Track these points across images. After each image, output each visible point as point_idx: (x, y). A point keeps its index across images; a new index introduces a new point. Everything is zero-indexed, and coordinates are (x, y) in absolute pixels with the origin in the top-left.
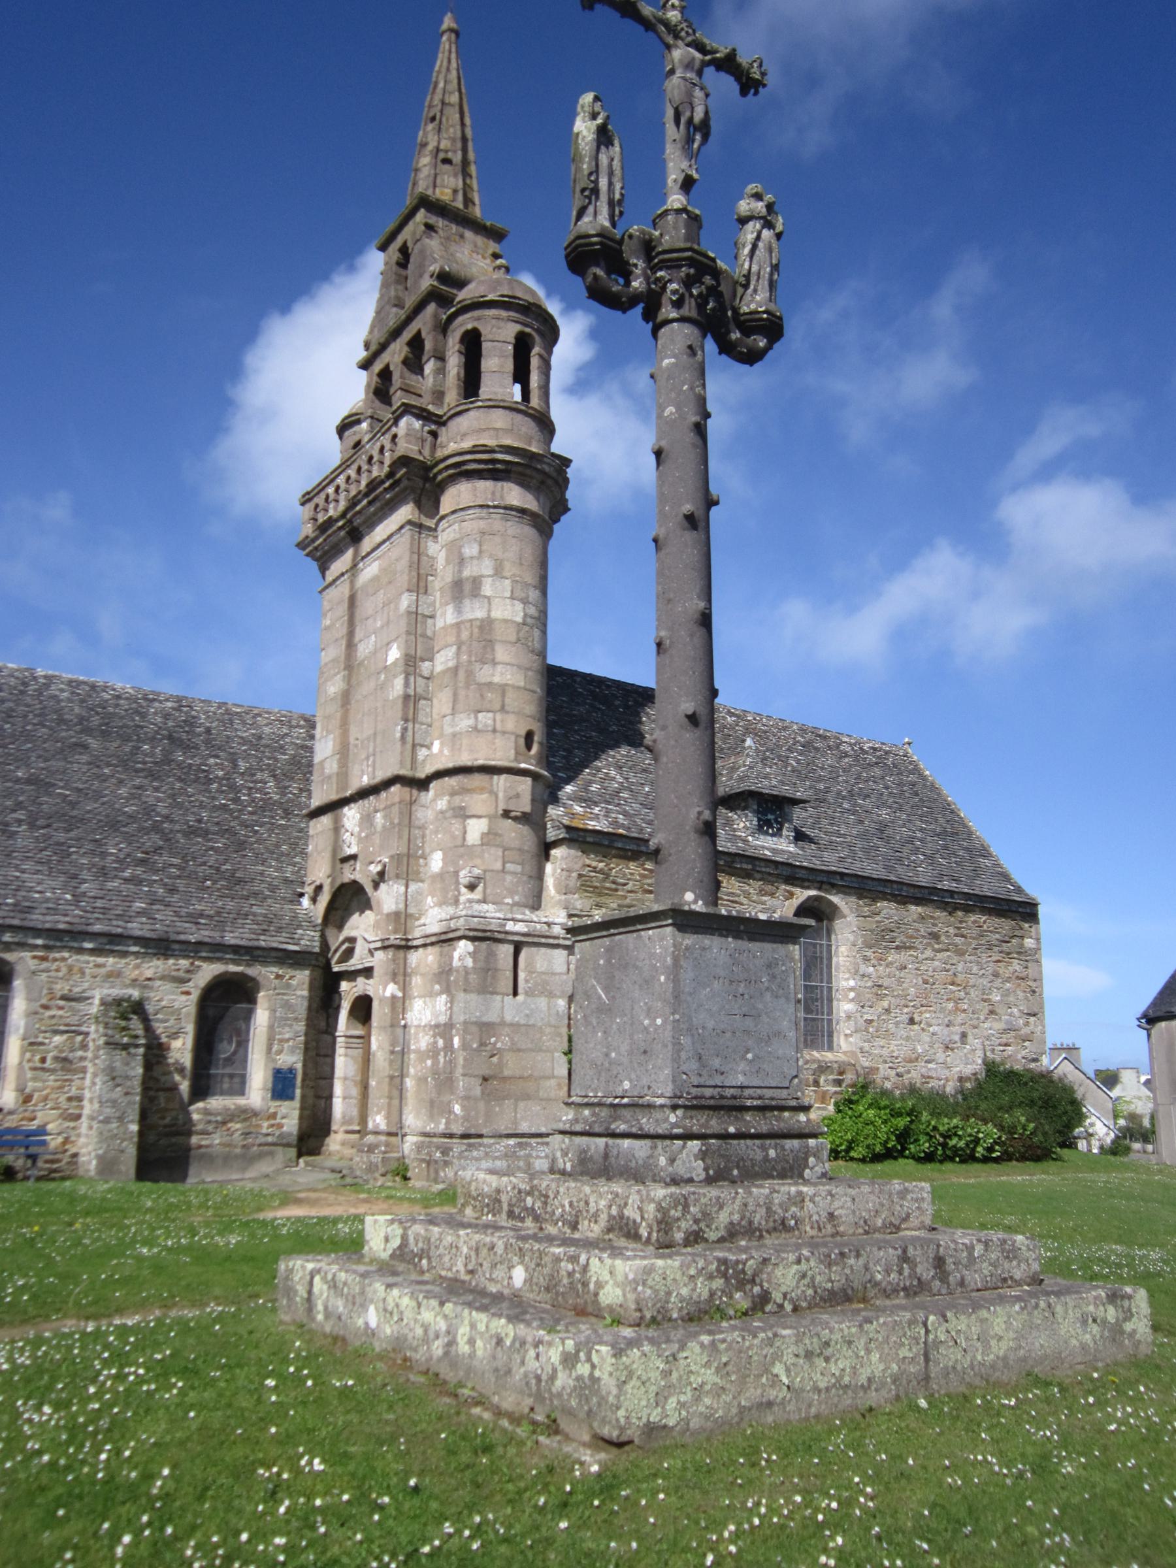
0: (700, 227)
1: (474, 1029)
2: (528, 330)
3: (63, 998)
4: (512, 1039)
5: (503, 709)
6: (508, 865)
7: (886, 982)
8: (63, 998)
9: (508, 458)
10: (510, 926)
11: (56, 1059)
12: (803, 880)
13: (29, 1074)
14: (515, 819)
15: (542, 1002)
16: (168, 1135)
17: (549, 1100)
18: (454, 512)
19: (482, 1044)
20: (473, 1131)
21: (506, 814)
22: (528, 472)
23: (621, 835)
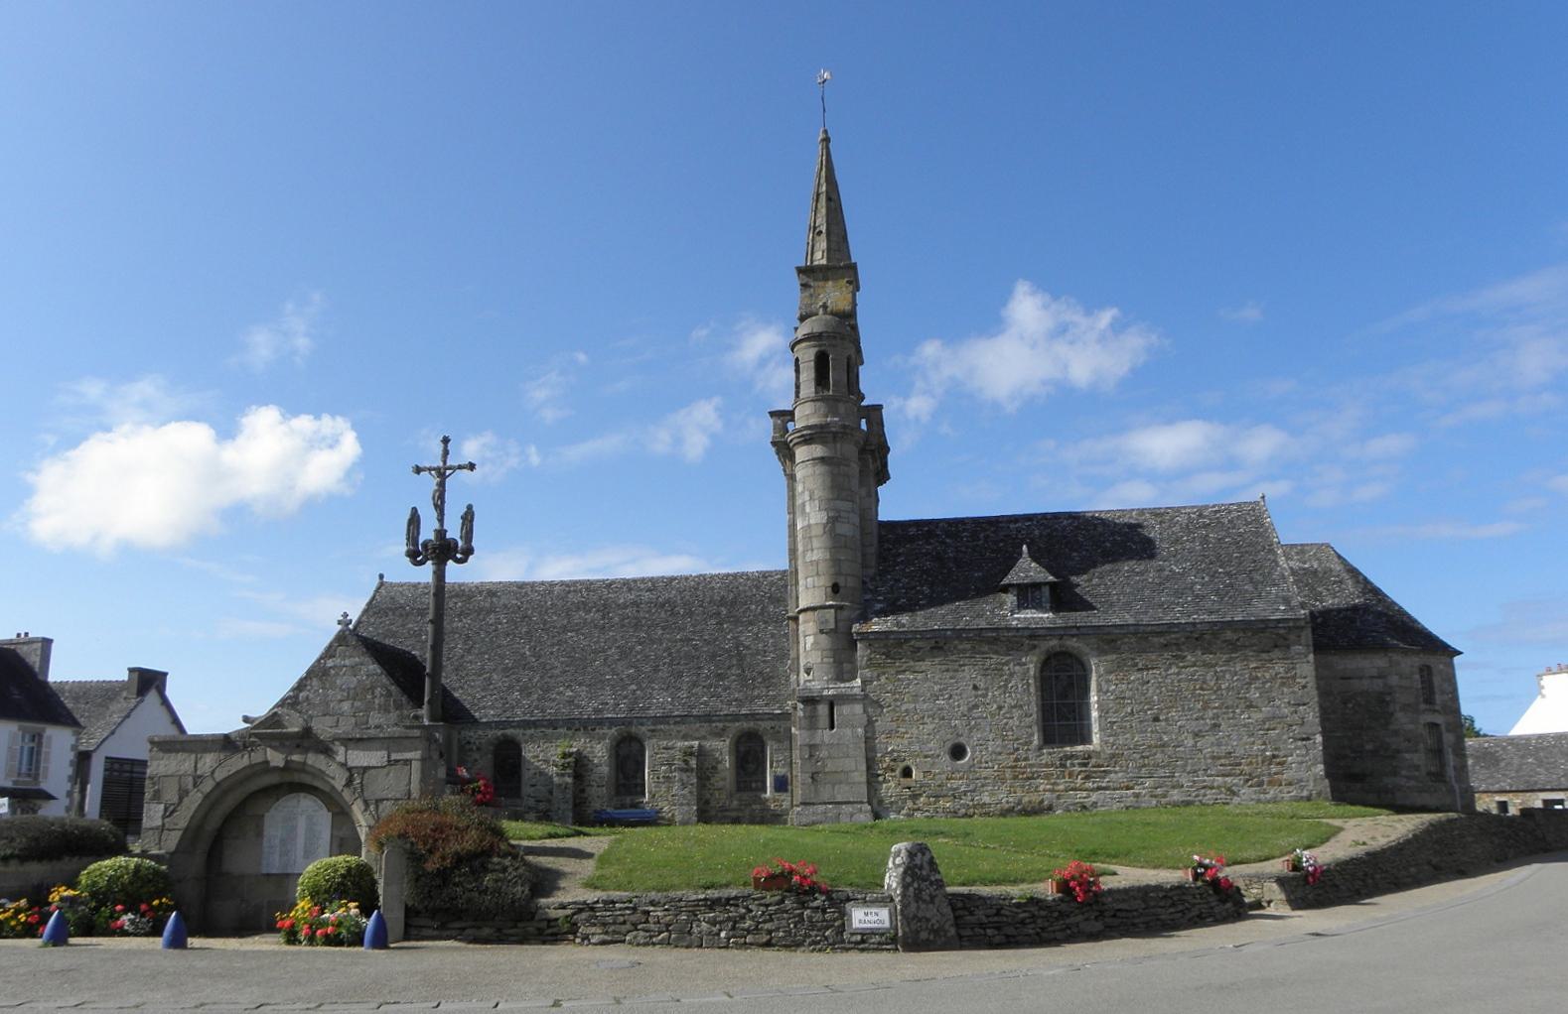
0: (857, 288)
1: (807, 748)
2: (823, 348)
3: (664, 748)
4: (829, 753)
5: (818, 574)
6: (825, 660)
7: (1128, 694)
8: (664, 748)
9: (809, 432)
10: (825, 693)
11: (664, 777)
12: (1045, 636)
13: (653, 785)
14: (826, 633)
15: (848, 732)
16: (721, 811)
17: (854, 783)
18: (803, 462)
19: (811, 756)
20: (808, 801)
21: (821, 632)
22: (823, 435)
23: (895, 632)
